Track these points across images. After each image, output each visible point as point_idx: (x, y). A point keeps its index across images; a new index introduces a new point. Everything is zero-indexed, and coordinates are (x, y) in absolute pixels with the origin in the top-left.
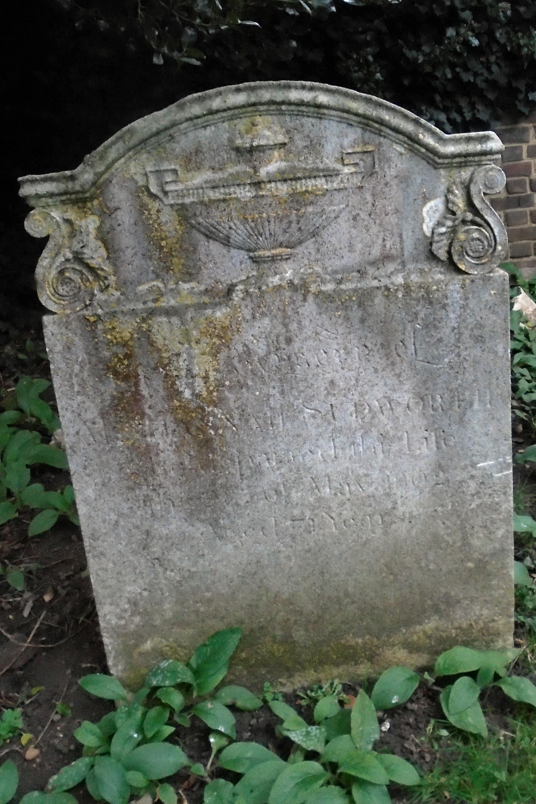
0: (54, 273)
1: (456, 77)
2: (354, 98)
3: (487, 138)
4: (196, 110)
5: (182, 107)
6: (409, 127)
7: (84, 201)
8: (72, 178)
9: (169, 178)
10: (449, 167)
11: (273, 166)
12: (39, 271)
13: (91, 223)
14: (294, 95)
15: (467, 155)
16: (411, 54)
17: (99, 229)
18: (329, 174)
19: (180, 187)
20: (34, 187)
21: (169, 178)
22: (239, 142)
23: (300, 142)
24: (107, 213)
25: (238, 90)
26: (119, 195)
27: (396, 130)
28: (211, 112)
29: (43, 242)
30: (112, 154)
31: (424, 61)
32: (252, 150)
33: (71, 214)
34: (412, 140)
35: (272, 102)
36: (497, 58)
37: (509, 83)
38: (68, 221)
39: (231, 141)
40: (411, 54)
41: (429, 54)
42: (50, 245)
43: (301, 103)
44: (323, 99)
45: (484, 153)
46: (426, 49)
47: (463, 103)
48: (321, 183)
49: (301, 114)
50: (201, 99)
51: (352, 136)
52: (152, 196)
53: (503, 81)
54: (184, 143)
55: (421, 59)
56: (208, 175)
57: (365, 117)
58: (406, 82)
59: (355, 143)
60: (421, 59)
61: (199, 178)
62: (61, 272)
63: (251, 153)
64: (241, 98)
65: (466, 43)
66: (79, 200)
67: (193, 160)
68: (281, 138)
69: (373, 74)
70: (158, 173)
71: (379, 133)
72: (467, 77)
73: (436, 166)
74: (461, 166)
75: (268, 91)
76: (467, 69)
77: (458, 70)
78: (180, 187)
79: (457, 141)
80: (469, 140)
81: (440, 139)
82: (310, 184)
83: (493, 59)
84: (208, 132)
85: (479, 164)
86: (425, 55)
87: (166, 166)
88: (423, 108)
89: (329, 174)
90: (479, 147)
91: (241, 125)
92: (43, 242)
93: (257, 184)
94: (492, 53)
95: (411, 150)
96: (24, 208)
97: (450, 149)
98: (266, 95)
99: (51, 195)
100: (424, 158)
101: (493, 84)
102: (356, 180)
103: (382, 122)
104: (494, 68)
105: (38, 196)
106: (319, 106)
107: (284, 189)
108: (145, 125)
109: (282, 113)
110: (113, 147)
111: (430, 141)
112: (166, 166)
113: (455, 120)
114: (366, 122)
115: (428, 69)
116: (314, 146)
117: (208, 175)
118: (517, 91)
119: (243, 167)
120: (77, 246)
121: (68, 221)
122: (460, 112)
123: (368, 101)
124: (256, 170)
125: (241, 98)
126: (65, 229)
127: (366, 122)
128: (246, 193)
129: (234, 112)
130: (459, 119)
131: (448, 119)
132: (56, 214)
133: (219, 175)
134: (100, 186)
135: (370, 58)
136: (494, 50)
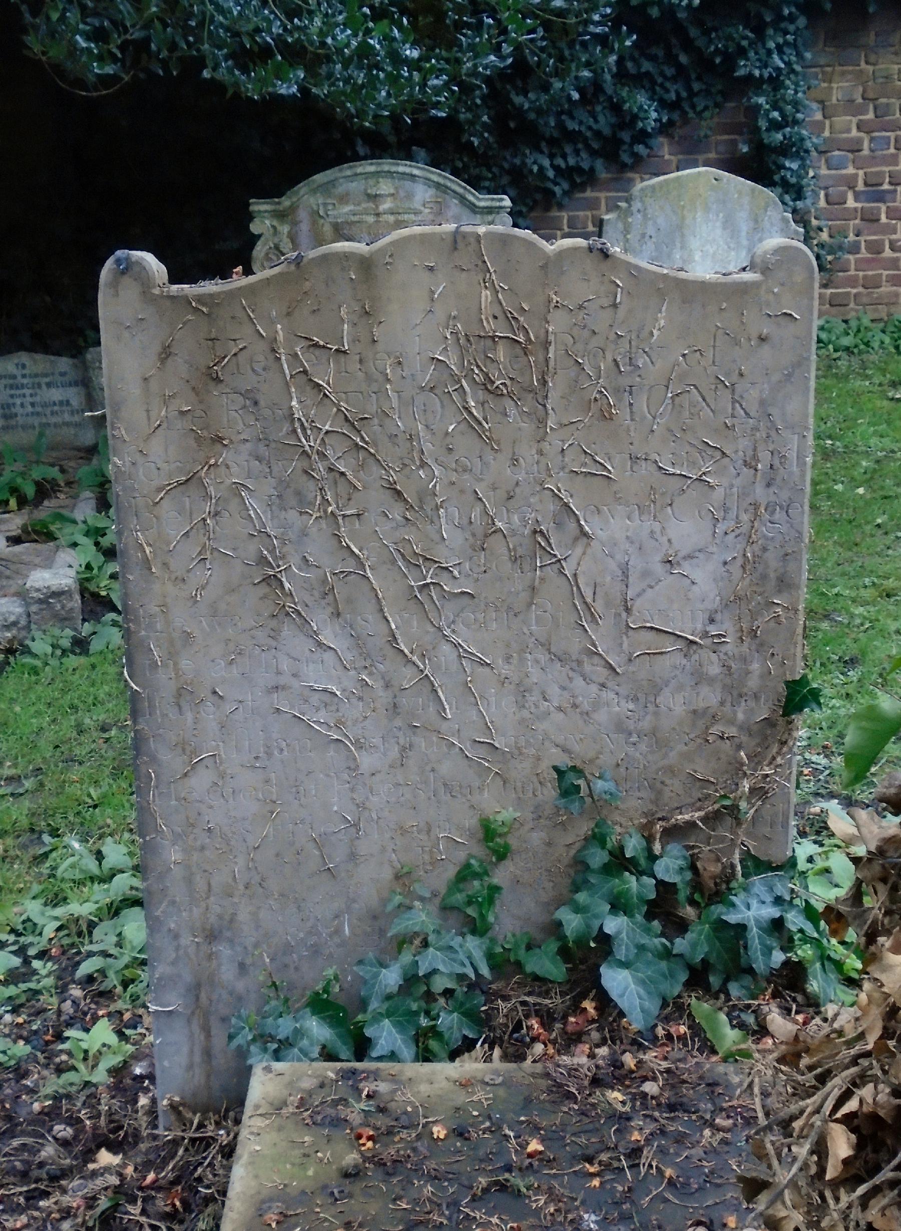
0: (263, 254)
1: (561, 126)
2: (432, 173)
3: (502, 200)
4: (349, 173)
5: (341, 170)
6: (460, 191)
7: (283, 216)
8: (279, 203)
9: (330, 207)
10: (482, 213)
11: (386, 205)
12: (255, 253)
13: (285, 229)
14: (401, 169)
15: (491, 208)
16: (518, 100)
17: (289, 233)
18: (417, 213)
19: (335, 212)
20: (259, 206)
21: (330, 207)
22: (369, 191)
23: (402, 194)
24: (295, 223)
25: (372, 164)
26: (303, 215)
27: (454, 191)
28: (356, 175)
29: (259, 236)
30: (302, 192)
31: (529, 108)
32: (376, 196)
33: (275, 223)
34: (462, 199)
35: (389, 172)
36: (604, 108)
37: (614, 134)
38: (273, 226)
39: (366, 190)
40: (518, 100)
41: (535, 102)
42: (262, 239)
43: (404, 174)
44: (416, 172)
45: (501, 207)
46: (531, 95)
47: (568, 149)
48: (412, 217)
49: (403, 179)
50: (350, 167)
51: (432, 192)
52: (322, 217)
53: (607, 131)
54: (340, 189)
55: (526, 106)
56: (351, 207)
57: (438, 183)
58: (512, 125)
59: (431, 197)
60: (526, 106)
61: (347, 209)
62: (267, 254)
63: (374, 198)
64: (372, 169)
65: (569, 97)
66: (281, 215)
67: (344, 199)
68: (392, 191)
69: (480, 117)
70: (325, 204)
71: (445, 192)
72: (572, 125)
73: (475, 213)
74: (490, 213)
75: (387, 165)
76: (572, 118)
77: (564, 117)
78: (335, 212)
79: (487, 199)
80: (493, 199)
81: (477, 198)
82: (406, 217)
83: (599, 108)
84: (354, 184)
85: (498, 213)
86: (531, 102)
87: (329, 201)
88: (527, 152)
89: (417, 213)
90: (498, 204)
91: (371, 182)
92: (259, 236)
93: (378, 215)
94: (599, 103)
95: (461, 202)
96: (250, 217)
97: (482, 204)
98: (386, 168)
99: (266, 211)
100: (468, 207)
101: (598, 134)
102: (431, 217)
103: (447, 187)
104: (601, 118)
105: (259, 211)
106: (415, 176)
107: (391, 218)
108: (319, 178)
109: (393, 178)
110: (302, 188)
111: (471, 198)
112: (329, 201)
113: (559, 166)
114: (438, 186)
115: (532, 116)
116: (410, 196)
117: (351, 207)
118: (621, 142)
119: (371, 205)
120: (276, 240)
121: (273, 226)
122: (564, 157)
123: (440, 175)
124: (377, 207)
125: (372, 169)
126: (271, 230)
127: (438, 186)
128: (371, 219)
129: (368, 175)
130: (563, 165)
131: (552, 165)
132: (267, 222)
133: (358, 208)
134: (293, 208)
135: (478, 101)
136: (601, 99)
